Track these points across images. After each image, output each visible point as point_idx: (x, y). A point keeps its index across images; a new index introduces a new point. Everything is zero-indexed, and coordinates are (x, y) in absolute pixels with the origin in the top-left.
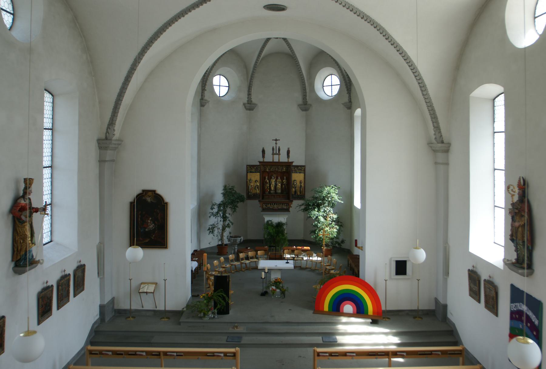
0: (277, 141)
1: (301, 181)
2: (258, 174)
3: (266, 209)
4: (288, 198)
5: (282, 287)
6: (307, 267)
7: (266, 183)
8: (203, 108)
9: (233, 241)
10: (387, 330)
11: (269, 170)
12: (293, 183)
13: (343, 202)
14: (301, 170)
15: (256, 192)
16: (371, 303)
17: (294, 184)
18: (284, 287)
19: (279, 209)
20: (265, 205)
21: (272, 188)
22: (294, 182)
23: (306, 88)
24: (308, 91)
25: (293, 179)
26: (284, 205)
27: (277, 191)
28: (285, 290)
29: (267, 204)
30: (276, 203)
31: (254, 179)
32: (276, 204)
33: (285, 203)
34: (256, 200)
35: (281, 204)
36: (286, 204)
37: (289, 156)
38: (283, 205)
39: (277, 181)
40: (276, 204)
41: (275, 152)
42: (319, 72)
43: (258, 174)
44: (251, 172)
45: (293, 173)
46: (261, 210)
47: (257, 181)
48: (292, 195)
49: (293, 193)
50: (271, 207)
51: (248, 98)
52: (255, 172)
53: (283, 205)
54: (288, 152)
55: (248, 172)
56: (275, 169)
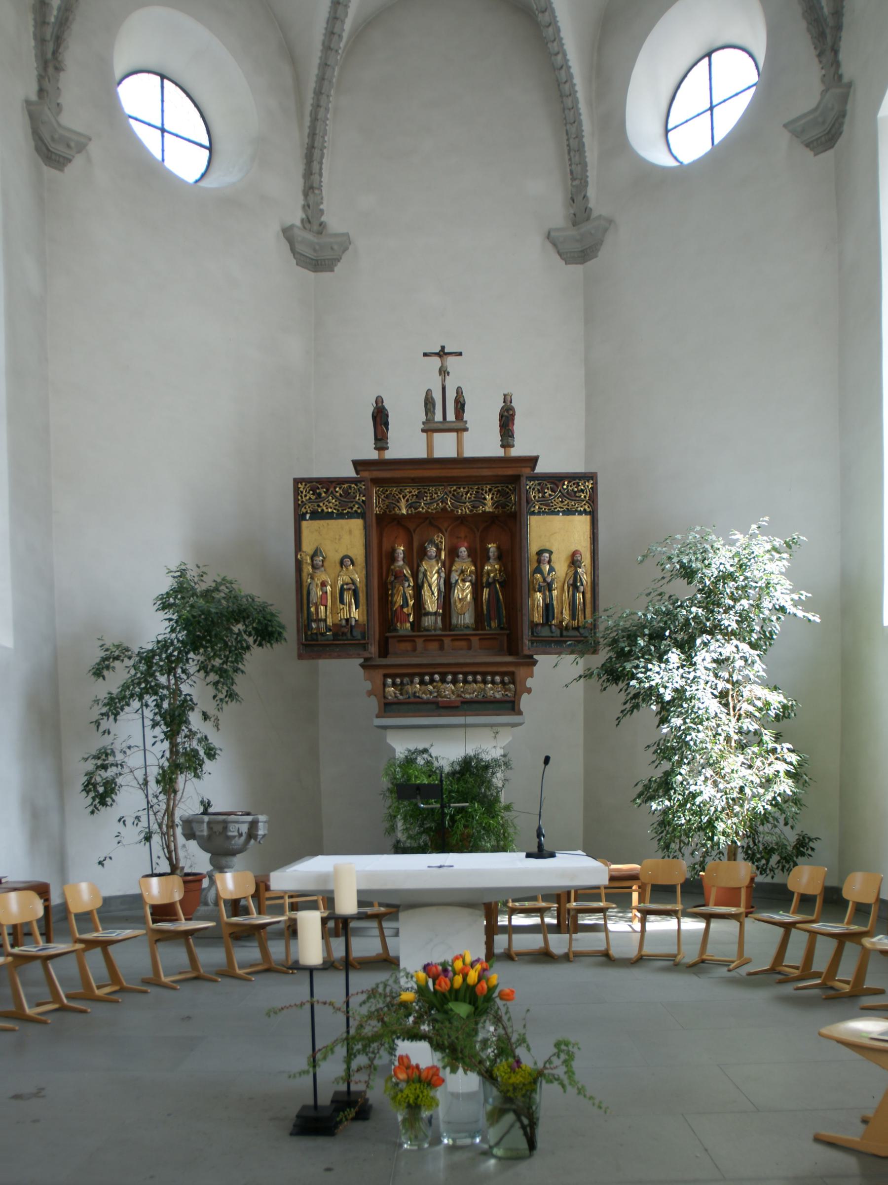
0: (450, 360)
1: (574, 554)
2: (357, 524)
3: (399, 703)
4: (512, 647)
5: (505, 1048)
6: (647, 950)
7: (400, 577)
8: (54, 172)
9: (205, 833)
11: (410, 506)
12: (535, 565)
13: (818, 620)
14: (572, 496)
17: (538, 570)
18: (520, 1052)
20: (394, 684)
21: (431, 604)
22: (539, 561)
23: (586, 140)
24: (592, 155)
25: (534, 547)
27: (454, 621)
28: (537, 1076)
29: (406, 680)
31: (333, 554)
32: (450, 677)
34: (349, 656)
35: (474, 674)
36: (502, 674)
37: (512, 436)
38: (485, 682)
39: (454, 568)
40: (450, 677)
41: (438, 417)
42: (657, 26)
43: (357, 524)
44: (317, 515)
45: (533, 513)
46: (376, 710)
47: (349, 562)
48: (534, 626)
49: (538, 618)
50: (424, 693)
51: (306, 207)
52: (341, 516)
53: (485, 682)
54: (507, 420)
56: (444, 501)
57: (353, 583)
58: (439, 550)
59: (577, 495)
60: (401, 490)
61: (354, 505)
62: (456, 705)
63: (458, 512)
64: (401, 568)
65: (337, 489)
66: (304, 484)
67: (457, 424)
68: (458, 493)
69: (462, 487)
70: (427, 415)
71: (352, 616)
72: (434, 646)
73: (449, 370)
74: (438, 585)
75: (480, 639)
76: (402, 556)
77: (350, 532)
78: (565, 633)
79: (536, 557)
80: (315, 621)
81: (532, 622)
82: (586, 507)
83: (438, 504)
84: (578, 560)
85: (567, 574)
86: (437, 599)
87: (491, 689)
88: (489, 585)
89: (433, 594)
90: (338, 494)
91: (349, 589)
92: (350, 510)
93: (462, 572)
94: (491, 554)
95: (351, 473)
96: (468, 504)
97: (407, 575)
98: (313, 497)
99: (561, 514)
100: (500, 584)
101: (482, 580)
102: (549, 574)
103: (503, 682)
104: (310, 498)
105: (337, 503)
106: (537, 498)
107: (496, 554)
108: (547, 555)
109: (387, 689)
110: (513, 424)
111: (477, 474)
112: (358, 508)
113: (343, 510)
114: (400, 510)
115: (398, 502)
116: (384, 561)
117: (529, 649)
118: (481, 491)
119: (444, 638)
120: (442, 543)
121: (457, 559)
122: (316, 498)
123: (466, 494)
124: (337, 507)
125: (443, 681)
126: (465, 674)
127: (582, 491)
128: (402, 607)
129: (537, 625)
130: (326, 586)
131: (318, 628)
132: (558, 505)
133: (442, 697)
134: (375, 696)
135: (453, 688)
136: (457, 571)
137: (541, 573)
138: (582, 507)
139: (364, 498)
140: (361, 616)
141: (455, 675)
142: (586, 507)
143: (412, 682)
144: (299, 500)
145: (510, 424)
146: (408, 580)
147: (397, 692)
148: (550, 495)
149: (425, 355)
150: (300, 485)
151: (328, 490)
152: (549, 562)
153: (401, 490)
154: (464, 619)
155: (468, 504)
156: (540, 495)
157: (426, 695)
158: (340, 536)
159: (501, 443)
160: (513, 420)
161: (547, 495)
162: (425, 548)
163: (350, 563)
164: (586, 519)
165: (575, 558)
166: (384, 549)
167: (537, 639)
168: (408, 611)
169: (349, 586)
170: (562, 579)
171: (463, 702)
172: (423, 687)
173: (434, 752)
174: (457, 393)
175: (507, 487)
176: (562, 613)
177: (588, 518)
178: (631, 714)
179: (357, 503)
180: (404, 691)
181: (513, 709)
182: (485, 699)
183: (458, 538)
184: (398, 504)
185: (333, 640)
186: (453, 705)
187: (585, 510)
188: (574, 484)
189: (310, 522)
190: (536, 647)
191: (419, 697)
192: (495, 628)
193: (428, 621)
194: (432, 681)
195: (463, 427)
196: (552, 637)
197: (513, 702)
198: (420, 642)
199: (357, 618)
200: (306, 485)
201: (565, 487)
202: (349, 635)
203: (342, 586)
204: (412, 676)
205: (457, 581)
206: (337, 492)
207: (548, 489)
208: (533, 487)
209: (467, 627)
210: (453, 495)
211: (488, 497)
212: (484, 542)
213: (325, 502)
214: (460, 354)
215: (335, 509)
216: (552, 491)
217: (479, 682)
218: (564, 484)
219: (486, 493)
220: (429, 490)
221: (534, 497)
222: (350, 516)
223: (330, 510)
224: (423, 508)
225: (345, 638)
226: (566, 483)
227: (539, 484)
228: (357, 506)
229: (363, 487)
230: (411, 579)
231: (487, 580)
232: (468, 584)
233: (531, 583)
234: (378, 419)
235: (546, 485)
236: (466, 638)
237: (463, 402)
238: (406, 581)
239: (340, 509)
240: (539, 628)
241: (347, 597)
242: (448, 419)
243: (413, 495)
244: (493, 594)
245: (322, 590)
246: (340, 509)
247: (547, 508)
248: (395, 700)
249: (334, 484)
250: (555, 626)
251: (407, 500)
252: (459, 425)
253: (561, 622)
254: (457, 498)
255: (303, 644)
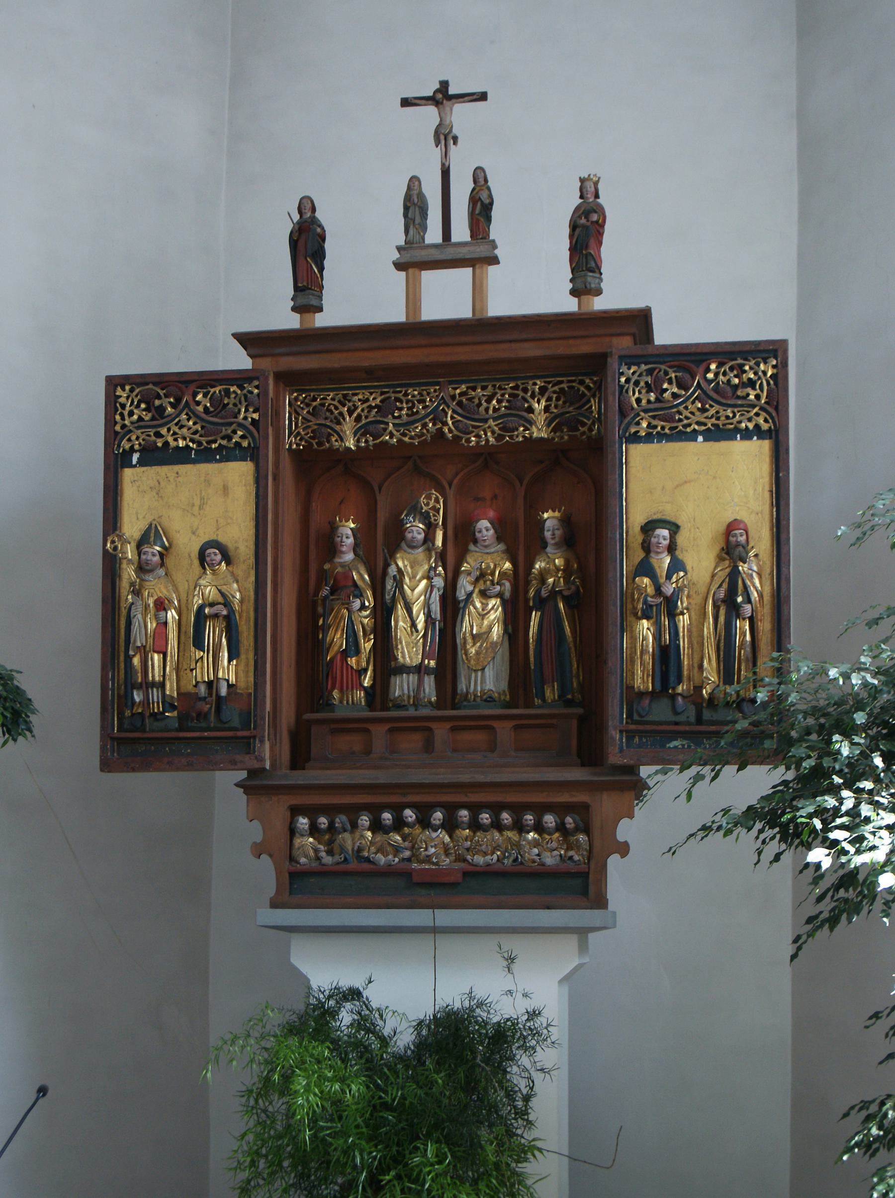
1: (731, 527)
3: (323, 873)
10: (118, 579)
11: (362, 431)
15: (204, 673)
16: (408, 925)
17: (645, 568)
19: (475, 875)
20: (314, 830)
22: (647, 547)
26: (539, 828)
27: (462, 686)
29: (341, 820)
30: (433, 807)
33: (549, 808)
35: (496, 809)
36: (561, 809)
37: (597, 269)
38: (520, 827)
41: (434, 235)
45: (635, 438)
46: (271, 890)
48: (633, 697)
50: (380, 850)
52: (206, 455)
55: (124, 460)
56: (438, 417)
57: (227, 604)
58: (430, 528)
59: (739, 393)
60: (345, 396)
61: (235, 432)
62: (452, 879)
63: (468, 441)
64: (346, 566)
65: (199, 397)
66: (127, 388)
67: (472, 249)
68: (470, 400)
69: (479, 385)
70: (407, 232)
71: (220, 675)
72: (411, 742)
73: (455, 131)
74: (427, 605)
75: (516, 728)
76: (350, 541)
77: (225, 489)
78: (707, 715)
79: (640, 538)
80: (139, 687)
81: (630, 688)
82: (761, 421)
83: (425, 426)
84: (738, 544)
85: (713, 576)
86: (425, 636)
87: (535, 844)
88: (541, 603)
89: (414, 625)
90: (200, 408)
91: (216, 616)
92: (224, 442)
93: (482, 576)
94: (548, 534)
95: (240, 360)
96: (491, 422)
97: (359, 583)
98: (147, 417)
99: (700, 438)
100: (567, 600)
101: (527, 592)
102: (669, 577)
103: (561, 828)
104: (140, 419)
105: (198, 427)
106: (644, 402)
107: (558, 533)
108: (665, 533)
109: (297, 841)
110: (600, 243)
111: (512, 355)
112: (243, 437)
113: (209, 442)
114: (342, 440)
115: (339, 423)
116: (313, 555)
117: (621, 750)
118: (521, 394)
119: (433, 725)
120: (438, 511)
121: (472, 547)
122: (153, 419)
123: (489, 401)
124: (197, 437)
125: (424, 823)
126: (475, 809)
127: (751, 384)
128: (345, 654)
129: (641, 694)
130: (165, 610)
131: (146, 702)
132: (694, 419)
133: (421, 862)
134: (271, 856)
135: (447, 839)
136: (469, 574)
137: (653, 577)
138: (750, 420)
139: (256, 416)
140: (241, 674)
141: (451, 809)
142: (761, 421)
143: (354, 826)
144: (116, 423)
145: (592, 242)
146: (360, 595)
147: (322, 847)
148: (675, 396)
149: (406, 103)
150: (119, 392)
151: (178, 400)
152: (671, 548)
153: (345, 396)
154: (483, 681)
155: (491, 422)
156: (652, 397)
157: (386, 855)
158: (202, 499)
159: (571, 286)
160: (601, 234)
161: (667, 395)
162: (402, 523)
163: (219, 557)
164: (761, 448)
165: (732, 539)
166: (313, 528)
167: (641, 727)
168: (358, 662)
169: (214, 610)
170: (703, 590)
171: (466, 874)
172: (379, 838)
173: (376, 996)
174: (475, 181)
175: (582, 382)
176: (701, 667)
177: (766, 445)
178: (831, 929)
179: (240, 425)
180: (336, 846)
181: (585, 892)
182: (520, 868)
183: (477, 499)
184: (337, 428)
185: (181, 729)
186: (446, 880)
187: (757, 426)
188: (732, 369)
189: (140, 470)
190: (640, 746)
191: (368, 860)
192: (554, 701)
193: (401, 686)
194: (399, 824)
195: (487, 254)
196: (676, 724)
197: (585, 876)
198: (379, 732)
199: (232, 679)
200: (132, 390)
201: (710, 376)
202: (212, 717)
203: (201, 608)
204: (353, 811)
205: (470, 595)
206: (198, 403)
207: (670, 382)
208: (635, 377)
209: (489, 700)
210: (460, 404)
211: (538, 407)
212: (533, 508)
213: (172, 425)
214: (483, 97)
215: (192, 441)
216: (680, 386)
217: (508, 828)
218: (708, 370)
219: (533, 396)
220: (406, 395)
221: (638, 401)
222: (227, 455)
223: (181, 443)
224: (392, 435)
225: (203, 725)
226: (713, 366)
227: (650, 372)
228: (240, 433)
229: (256, 391)
230: (369, 593)
231: (538, 592)
232: (492, 602)
233: (626, 598)
234: (301, 244)
235: (666, 373)
236: (483, 724)
237: (487, 201)
238: (355, 596)
239: (204, 440)
240: (646, 702)
241: (213, 632)
242: (455, 238)
243: (371, 408)
244: (551, 625)
245: (156, 617)
246: (204, 440)
247: (668, 425)
248: (314, 864)
249: (192, 387)
250: (684, 697)
251: (358, 419)
252: (481, 250)
253: (699, 689)
254: (467, 409)
255: (113, 739)
